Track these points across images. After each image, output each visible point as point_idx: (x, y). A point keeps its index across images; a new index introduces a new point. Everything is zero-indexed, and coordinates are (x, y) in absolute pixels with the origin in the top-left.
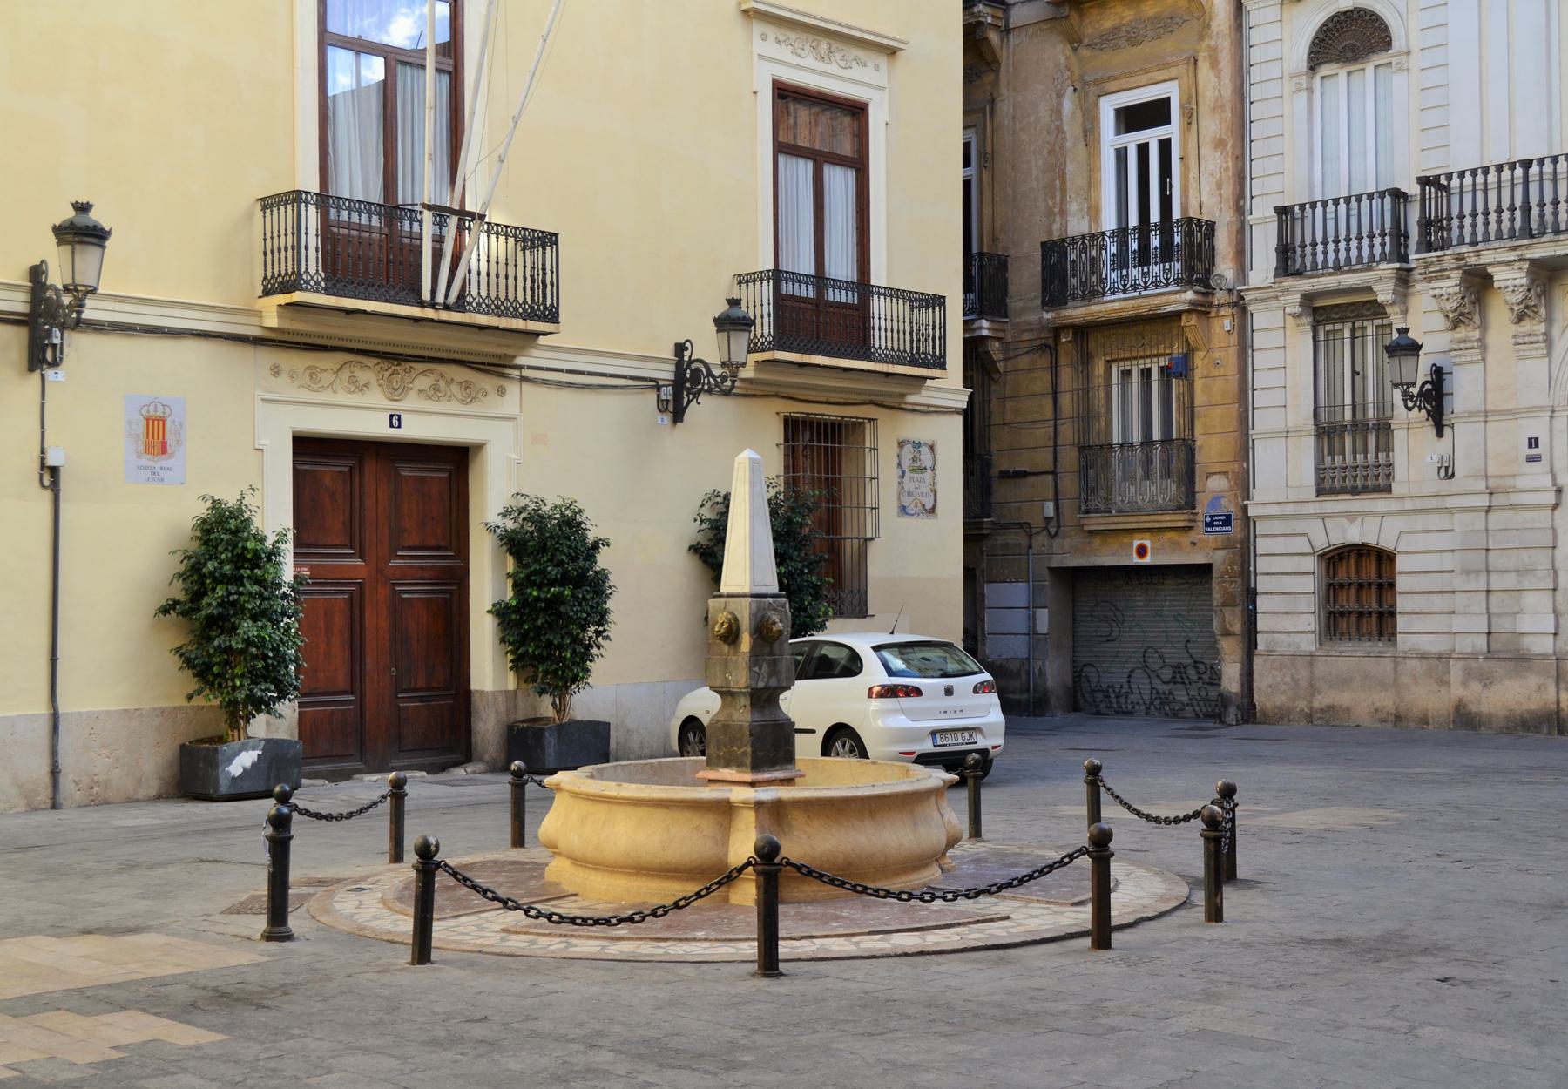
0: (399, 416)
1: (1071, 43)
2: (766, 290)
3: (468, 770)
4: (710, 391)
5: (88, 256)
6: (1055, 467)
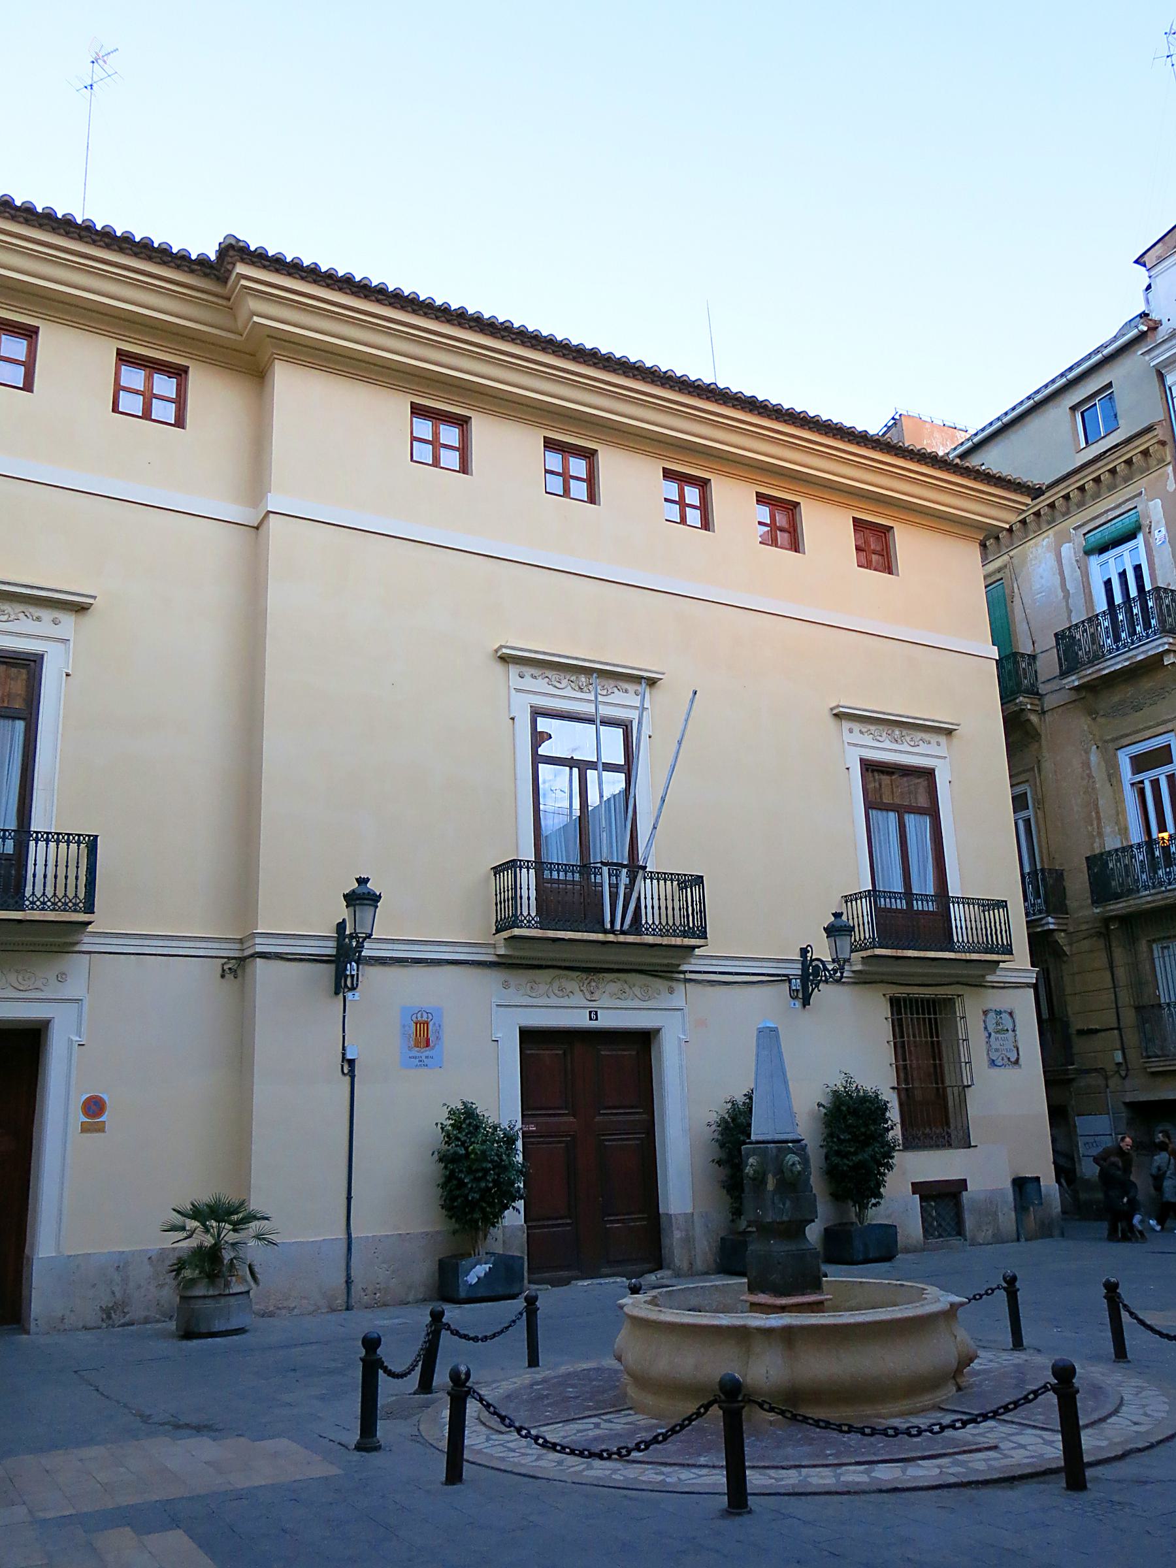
0: (596, 1012)
1: (1090, 714)
2: (864, 906)
3: (658, 1276)
4: (826, 981)
5: (365, 913)
6: (1119, 1023)
